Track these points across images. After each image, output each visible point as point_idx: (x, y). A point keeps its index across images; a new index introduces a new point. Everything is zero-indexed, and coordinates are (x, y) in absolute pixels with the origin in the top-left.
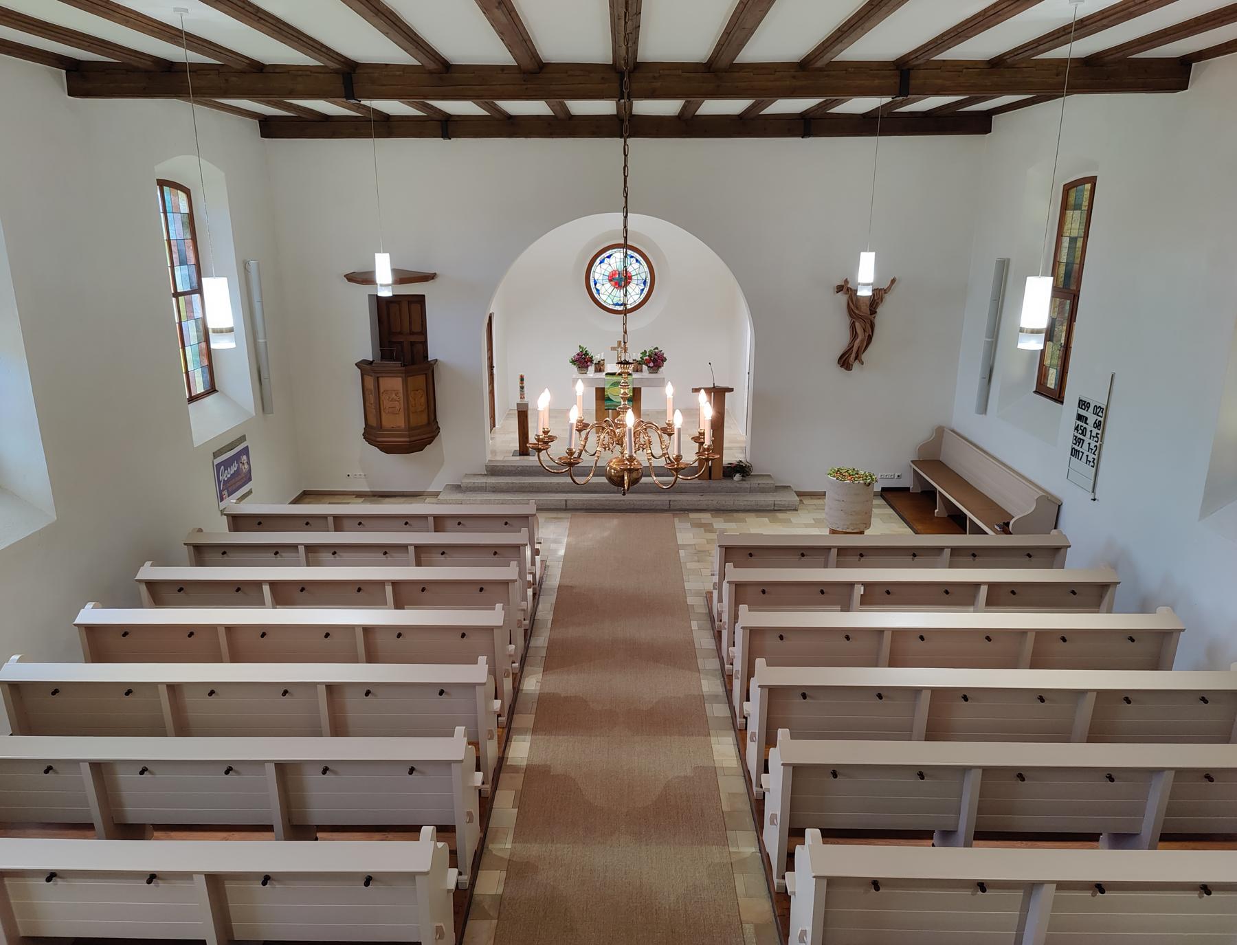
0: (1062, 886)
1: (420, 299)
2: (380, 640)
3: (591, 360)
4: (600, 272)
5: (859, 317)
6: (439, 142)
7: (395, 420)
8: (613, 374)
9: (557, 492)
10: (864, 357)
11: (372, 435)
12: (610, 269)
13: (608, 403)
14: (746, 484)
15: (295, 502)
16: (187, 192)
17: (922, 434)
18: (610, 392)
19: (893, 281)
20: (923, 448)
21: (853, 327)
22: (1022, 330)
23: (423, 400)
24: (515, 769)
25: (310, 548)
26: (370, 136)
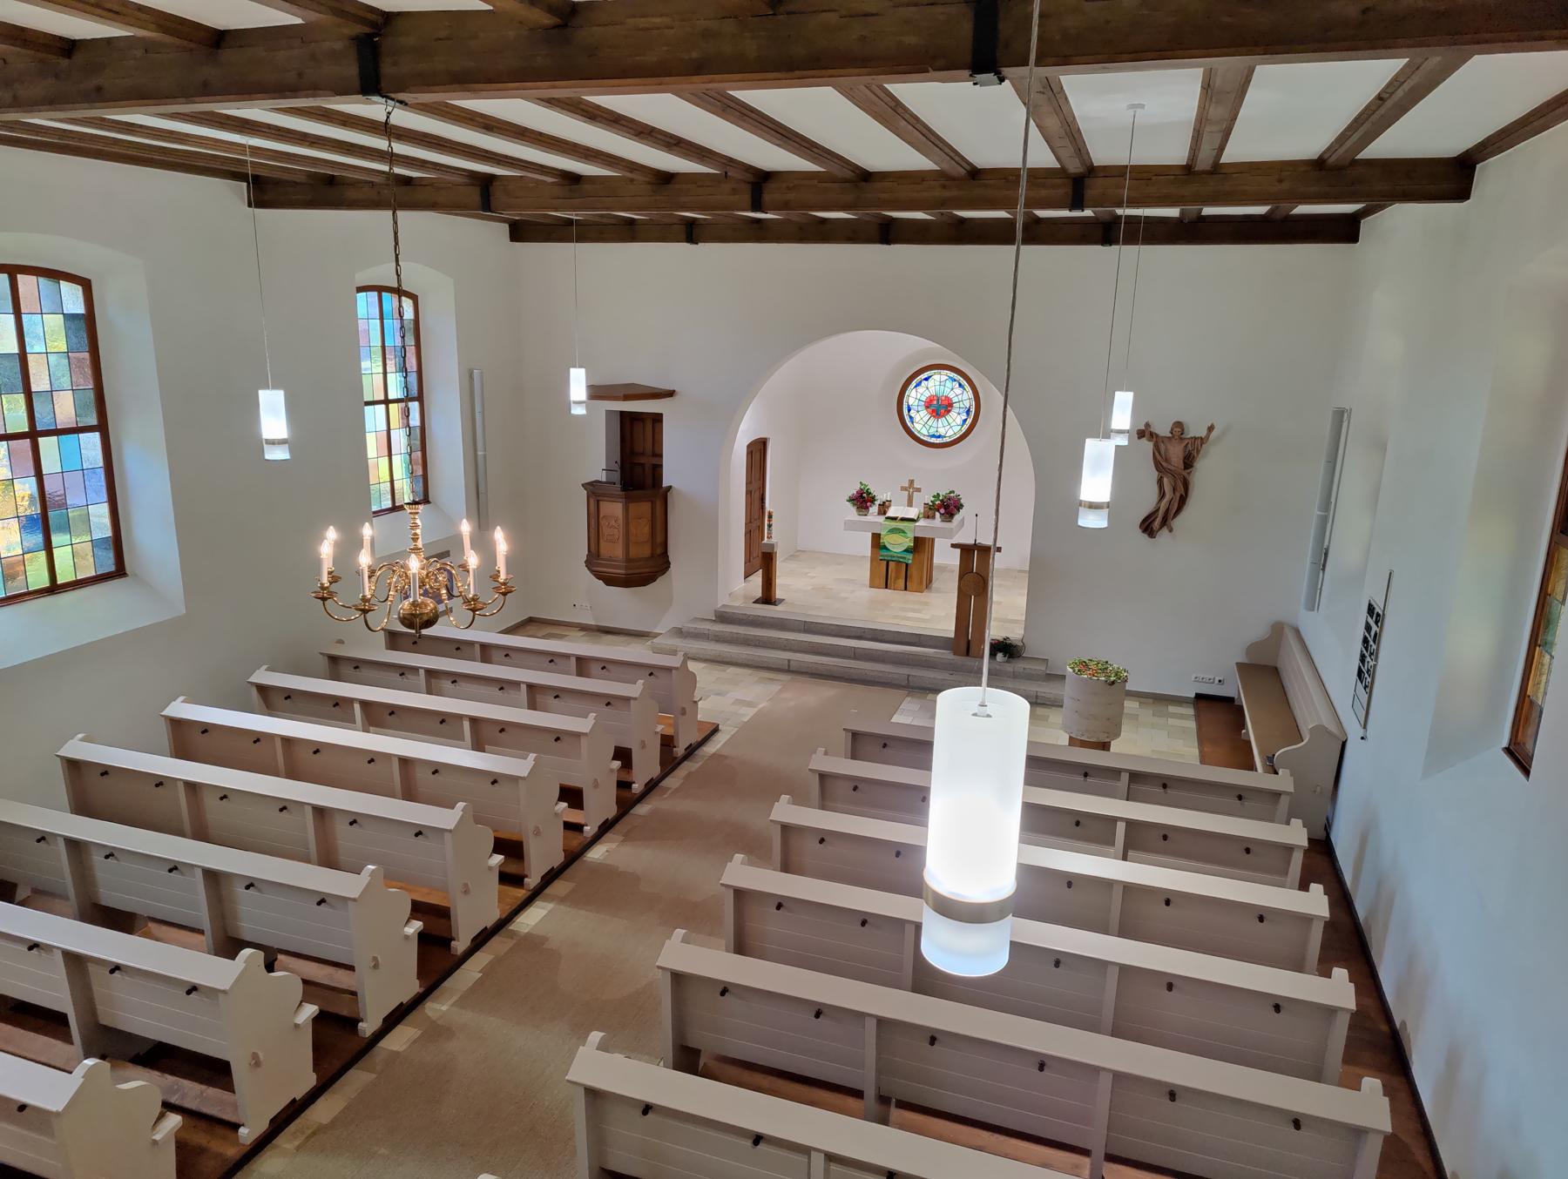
0: (831, 1158)
1: (657, 419)
2: (422, 776)
3: (873, 500)
4: (915, 396)
5: (1172, 473)
6: (684, 248)
7: (614, 550)
8: (894, 519)
9: (785, 649)
10: (1177, 523)
11: (594, 561)
12: (927, 394)
13: (884, 552)
14: (1009, 667)
15: (507, 631)
16: (414, 298)
17: (1257, 630)
18: (887, 540)
19: (1211, 429)
20: (1253, 648)
21: (1160, 482)
22: (1081, 503)
23: (647, 530)
24: (513, 934)
25: (431, 673)
26: (571, 241)
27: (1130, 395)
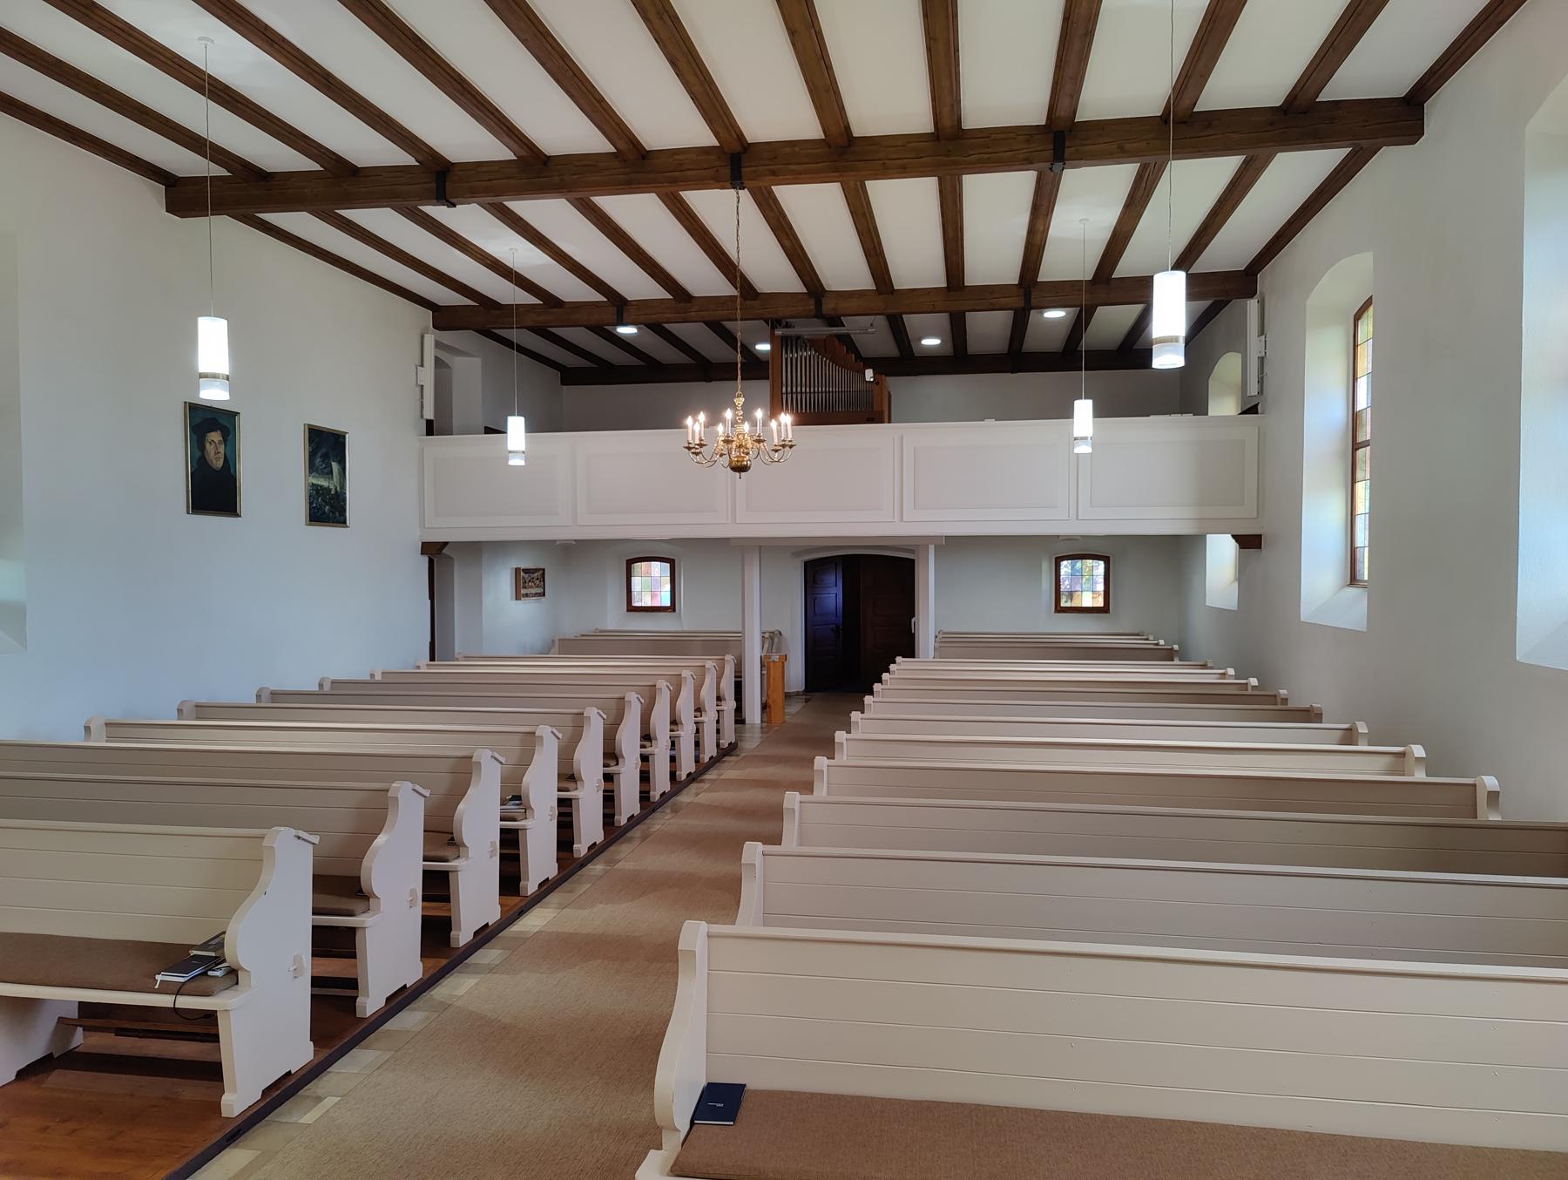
27: (1089, 403)
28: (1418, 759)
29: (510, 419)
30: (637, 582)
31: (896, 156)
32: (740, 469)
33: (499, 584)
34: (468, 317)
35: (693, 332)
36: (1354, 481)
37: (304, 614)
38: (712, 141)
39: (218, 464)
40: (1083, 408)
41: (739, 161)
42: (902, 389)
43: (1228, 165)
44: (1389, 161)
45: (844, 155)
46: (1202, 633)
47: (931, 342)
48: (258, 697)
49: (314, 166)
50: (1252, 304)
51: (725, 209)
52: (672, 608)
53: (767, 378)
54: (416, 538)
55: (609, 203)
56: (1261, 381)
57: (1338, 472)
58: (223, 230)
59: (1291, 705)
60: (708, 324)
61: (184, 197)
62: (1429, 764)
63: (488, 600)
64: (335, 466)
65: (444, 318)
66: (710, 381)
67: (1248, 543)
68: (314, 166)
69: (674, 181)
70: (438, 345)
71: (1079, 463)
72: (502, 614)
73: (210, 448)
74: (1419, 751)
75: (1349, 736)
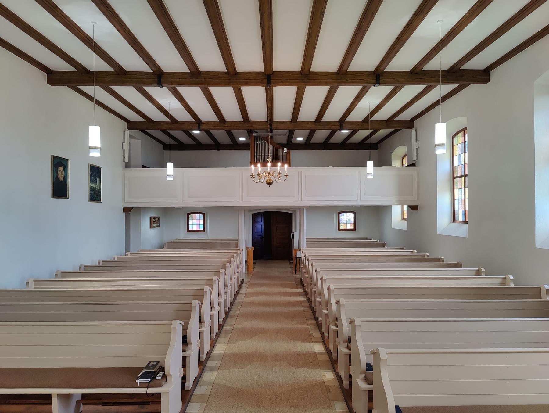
27: (172, 164)
28: (511, 280)
29: (168, 163)
30: (191, 222)
31: (251, 79)
32: (270, 183)
33: (146, 222)
34: (142, 126)
35: (179, 135)
36: (454, 189)
37: (86, 235)
38: (187, 70)
39: (62, 179)
40: (370, 163)
41: (196, 77)
42: (295, 154)
43: (388, 89)
44: (473, 91)
45: (233, 77)
46: (389, 237)
47: (242, 139)
48: (80, 268)
49: (74, 70)
50: (414, 131)
51: (193, 94)
52: (204, 231)
53: (249, 150)
54: (121, 206)
55: (181, 89)
56: (417, 156)
57: (448, 186)
58: (64, 91)
59: (445, 262)
60: (184, 131)
61: (54, 78)
62: (514, 281)
63: (142, 228)
64: (97, 179)
65: (131, 125)
66: (219, 150)
67: (413, 208)
68: (74, 70)
69: (172, 83)
70: (131, 137)
71: (368, 181)
72: (148, 234)
73: (59, 173)
74: (511, 277)
75: (478, 273)
